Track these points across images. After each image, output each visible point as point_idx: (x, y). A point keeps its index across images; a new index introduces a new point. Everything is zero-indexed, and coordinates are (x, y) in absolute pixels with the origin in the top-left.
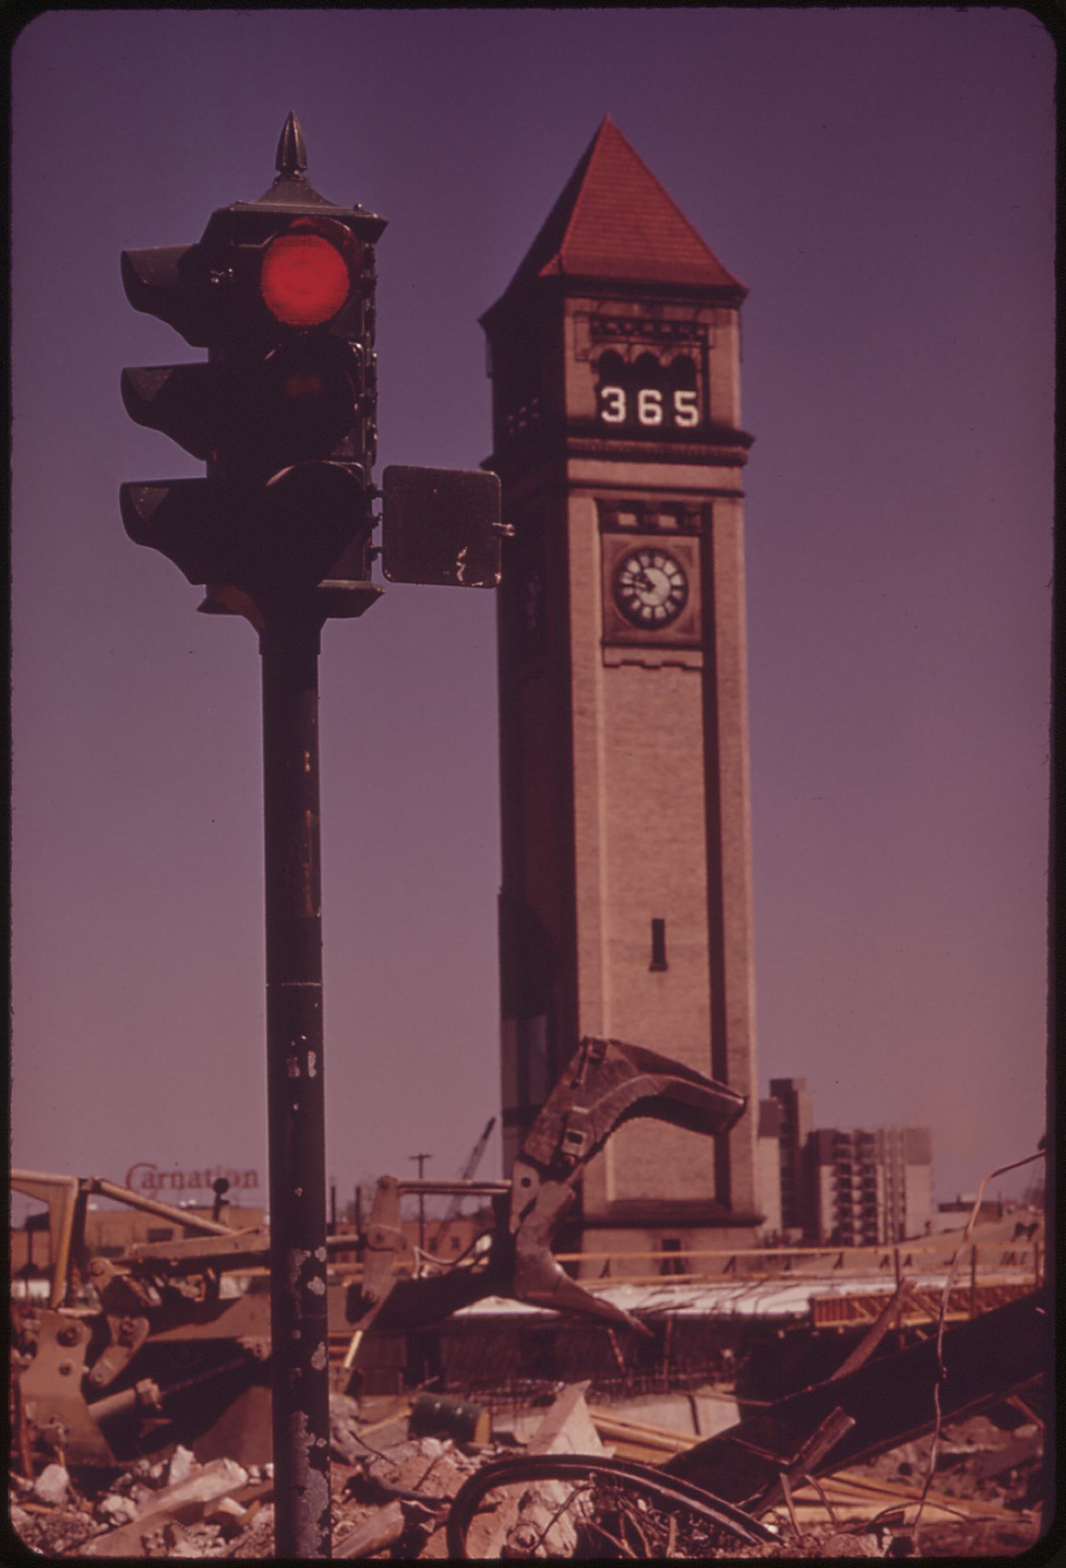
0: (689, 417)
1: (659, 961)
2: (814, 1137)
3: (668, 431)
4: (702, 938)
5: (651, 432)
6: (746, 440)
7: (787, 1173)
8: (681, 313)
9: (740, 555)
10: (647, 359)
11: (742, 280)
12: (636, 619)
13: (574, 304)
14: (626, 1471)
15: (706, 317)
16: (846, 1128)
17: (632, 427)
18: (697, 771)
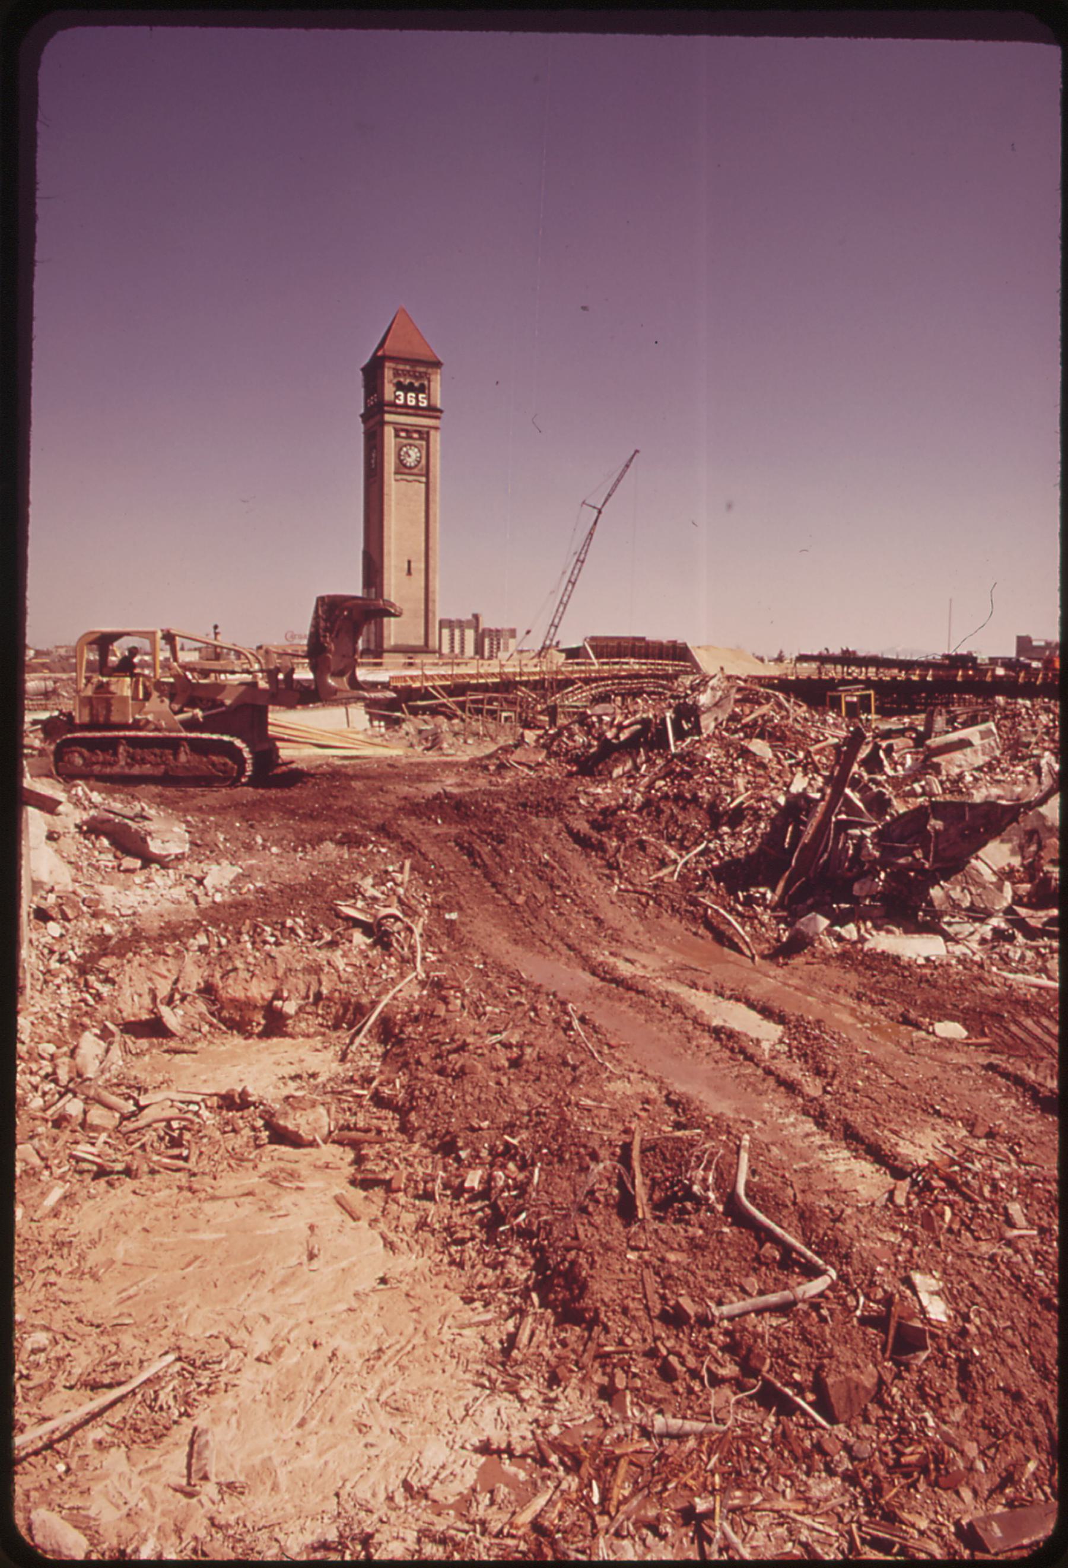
0: (424, 404)
1: (409, 573)
2: (484, 630)
3: (417, 407)
4: (423, 566)
5: (423, 409)
6: (441, 411)
7: (476, 640)
8: (422, 369)
9: (438, 447)
10: (411, 384)
11: (442, 360)
12: (405, 466)
13: (387, 364)
14: (90, 731)
15: (430, 371)
16: (493, 627)
17: (406, 406)
18: (423, 514)
